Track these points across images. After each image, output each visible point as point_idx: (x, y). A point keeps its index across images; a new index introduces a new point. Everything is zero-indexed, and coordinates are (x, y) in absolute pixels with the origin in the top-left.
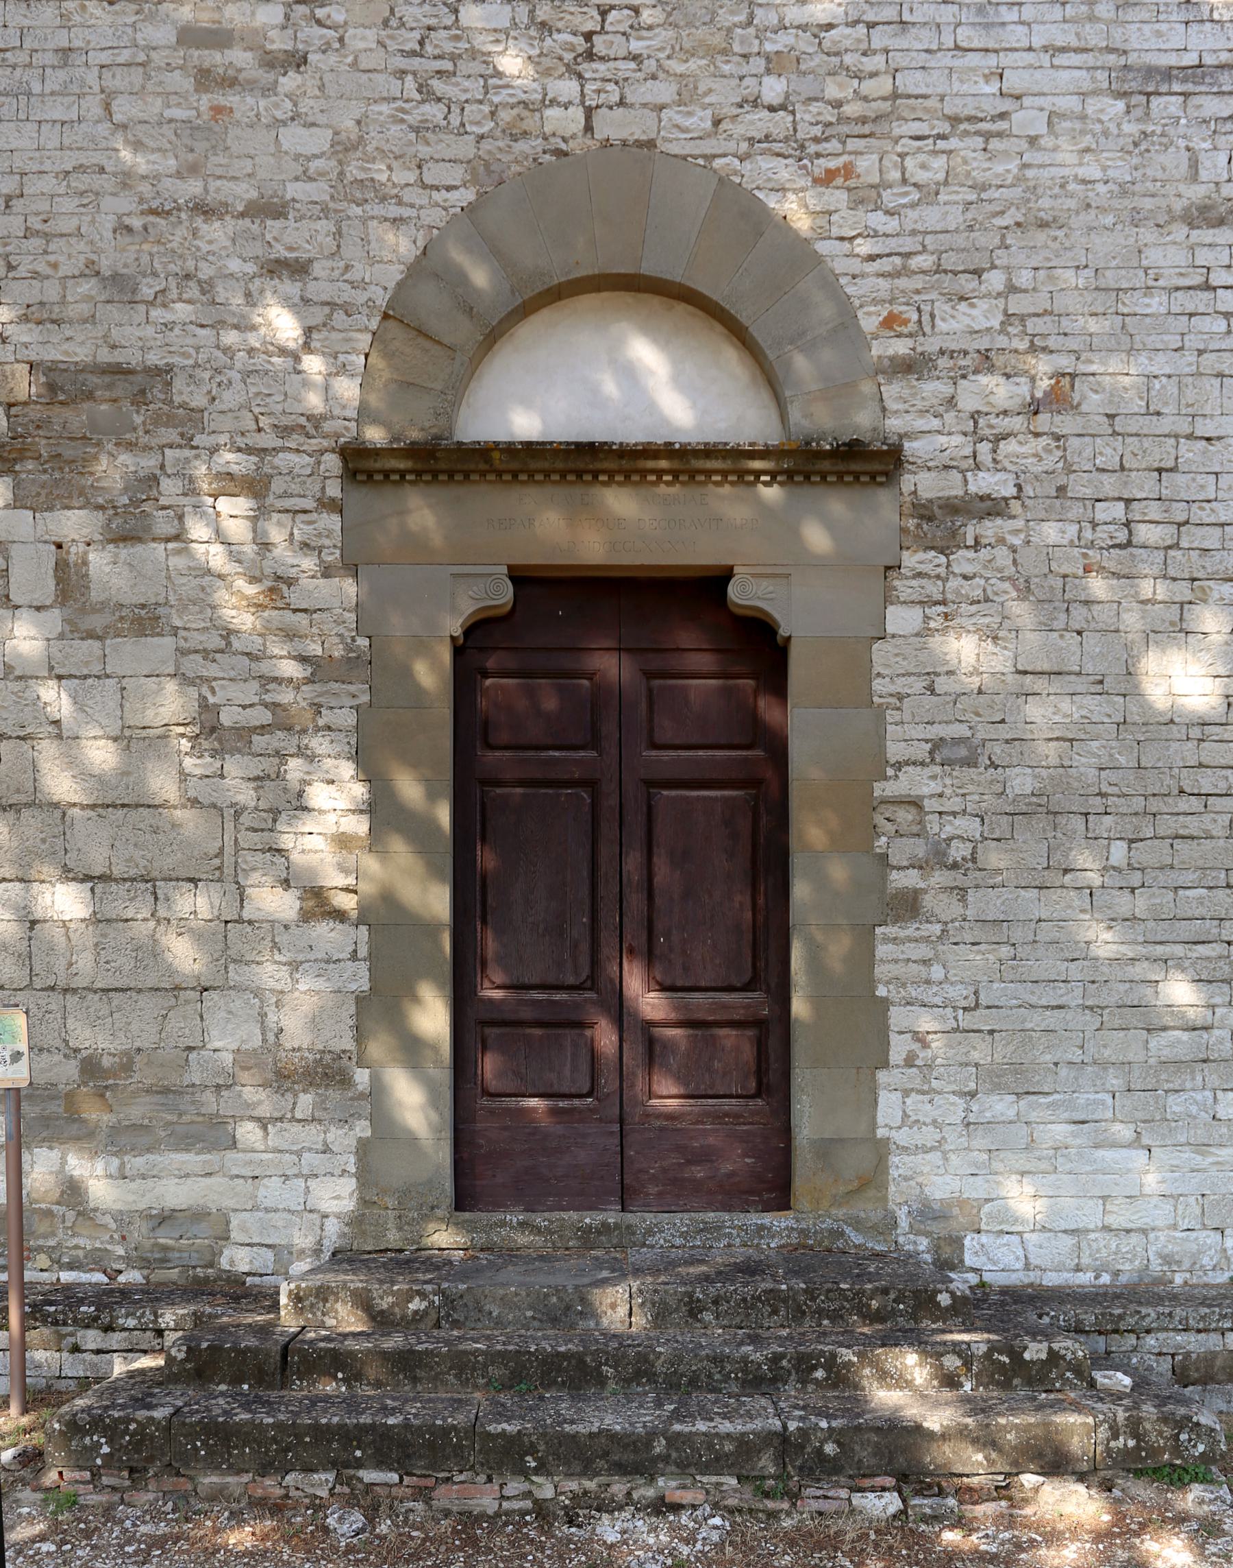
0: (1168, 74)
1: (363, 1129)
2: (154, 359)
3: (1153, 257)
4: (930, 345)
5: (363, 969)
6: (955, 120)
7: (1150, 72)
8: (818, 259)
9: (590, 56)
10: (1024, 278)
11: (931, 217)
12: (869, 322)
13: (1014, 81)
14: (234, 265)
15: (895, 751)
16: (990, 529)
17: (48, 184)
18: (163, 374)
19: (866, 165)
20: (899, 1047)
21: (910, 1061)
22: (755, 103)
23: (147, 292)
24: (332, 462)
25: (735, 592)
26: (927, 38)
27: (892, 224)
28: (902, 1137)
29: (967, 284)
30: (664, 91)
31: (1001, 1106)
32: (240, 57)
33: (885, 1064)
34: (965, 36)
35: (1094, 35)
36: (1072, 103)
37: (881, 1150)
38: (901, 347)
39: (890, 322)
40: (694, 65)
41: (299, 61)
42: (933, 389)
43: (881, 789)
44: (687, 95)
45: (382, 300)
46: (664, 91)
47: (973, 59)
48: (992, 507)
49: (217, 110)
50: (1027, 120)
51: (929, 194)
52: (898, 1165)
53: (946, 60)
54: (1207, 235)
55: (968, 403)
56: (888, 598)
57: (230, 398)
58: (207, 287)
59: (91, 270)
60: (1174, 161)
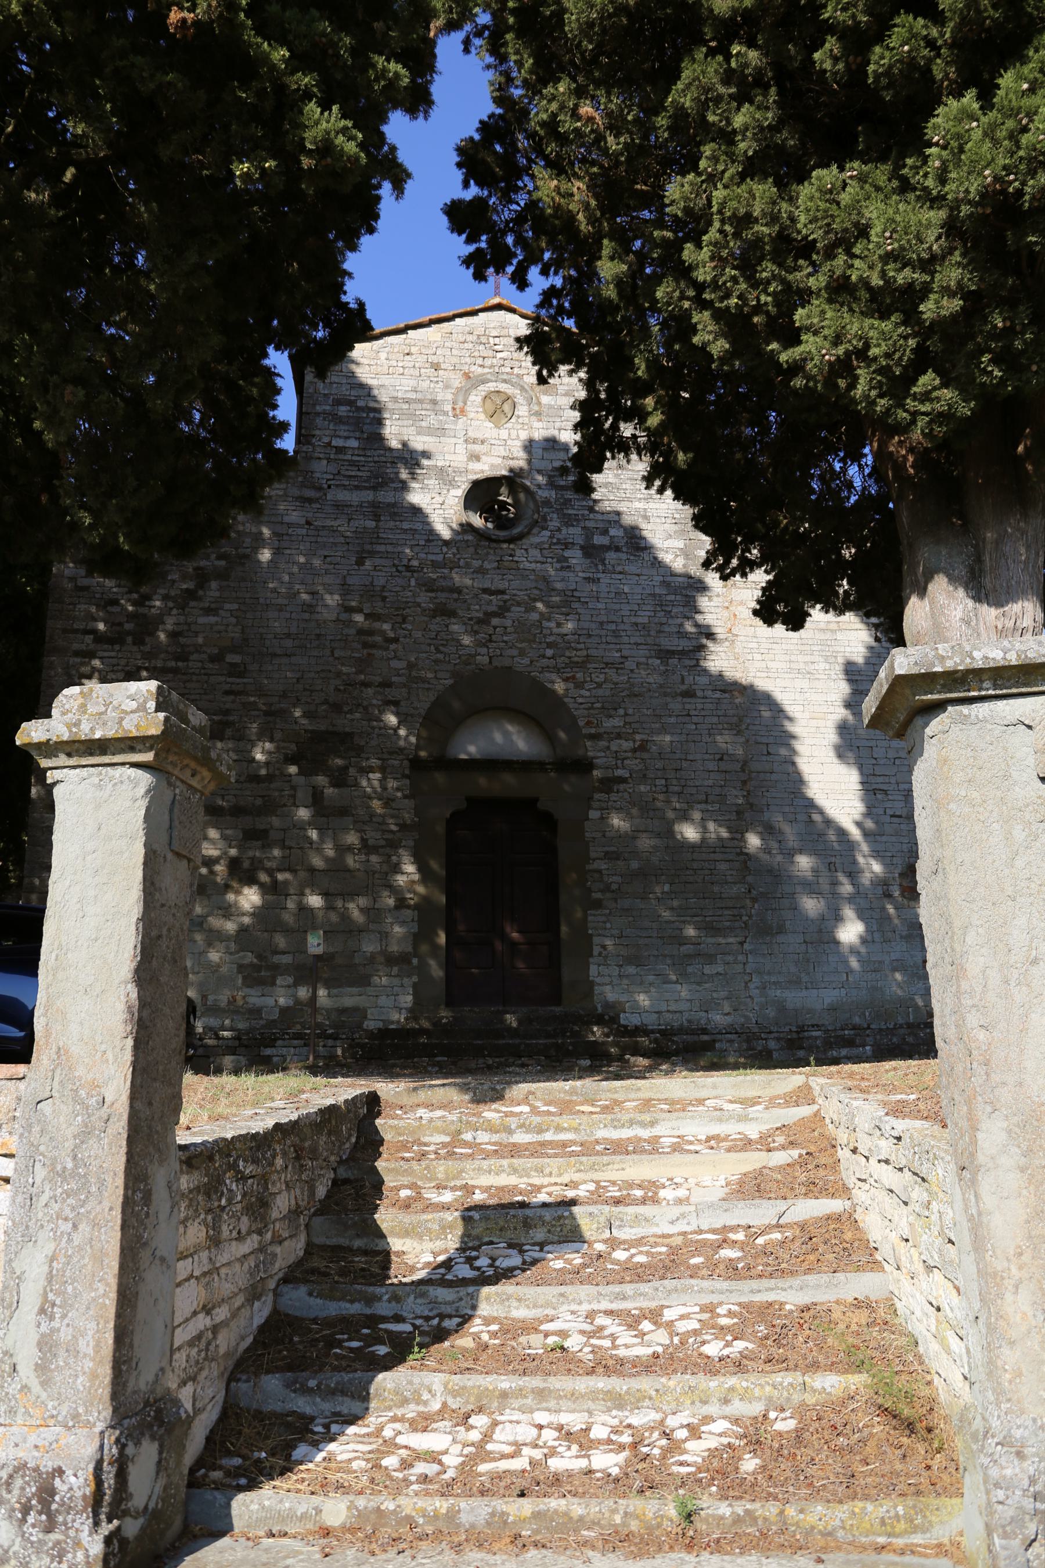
0: (673, 652)
1: (415, 979)
2: (347, 729)
3: (671, 706)
4: (602, 730)
5: (416, 925)
6: (607, 664)
7: (668, 651)
8: (564, 704)
9: (491, 641)
10: (630, 711)
11: (600, 692)
12: (581, 723)
13: (625, 653)
14: (375, 702)
15: (593, 855)
16: (622, 787)
17: (312, 675)
18: (350, 735)
19: (578, 675)
20: (596, 950)
21: (600, 954)
22: (544, 656)
23: (346, 709)
24: (406, 763)
25: (539, 805)
26: (597, 640)
27: (588, 694)
28: (598, 980)
29: (613, 712)
30: (515, 652)
31: (631, 970)
32: (378, 639)
33: (591, 955)
34: (609, 639)
35: (650, 640)
36: (643, 660)
37: (592, 984)
38: (593, 731)
39: (588, 723)
40: (524, 645)
41: (396, 640)
42: (603, 744)
43: (588, 867)
44: (522, 653)
45: (423, 712)
46: (515, 652)
47: (612, 646)
48: (622, 780)
49: (369, 654)
50: (630, 664)
51: (599, 685)
52: (597, 989)
53: (604, 646)
54: (688, 700)
55: (614, 748)
56: (590, 808)
57: (373, 743)
58: (366, 708)
59: (326, 702)
60: (677, 678)
